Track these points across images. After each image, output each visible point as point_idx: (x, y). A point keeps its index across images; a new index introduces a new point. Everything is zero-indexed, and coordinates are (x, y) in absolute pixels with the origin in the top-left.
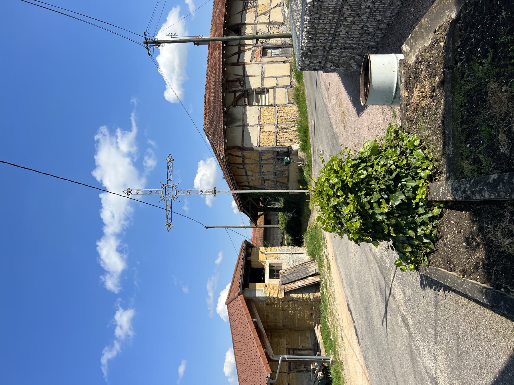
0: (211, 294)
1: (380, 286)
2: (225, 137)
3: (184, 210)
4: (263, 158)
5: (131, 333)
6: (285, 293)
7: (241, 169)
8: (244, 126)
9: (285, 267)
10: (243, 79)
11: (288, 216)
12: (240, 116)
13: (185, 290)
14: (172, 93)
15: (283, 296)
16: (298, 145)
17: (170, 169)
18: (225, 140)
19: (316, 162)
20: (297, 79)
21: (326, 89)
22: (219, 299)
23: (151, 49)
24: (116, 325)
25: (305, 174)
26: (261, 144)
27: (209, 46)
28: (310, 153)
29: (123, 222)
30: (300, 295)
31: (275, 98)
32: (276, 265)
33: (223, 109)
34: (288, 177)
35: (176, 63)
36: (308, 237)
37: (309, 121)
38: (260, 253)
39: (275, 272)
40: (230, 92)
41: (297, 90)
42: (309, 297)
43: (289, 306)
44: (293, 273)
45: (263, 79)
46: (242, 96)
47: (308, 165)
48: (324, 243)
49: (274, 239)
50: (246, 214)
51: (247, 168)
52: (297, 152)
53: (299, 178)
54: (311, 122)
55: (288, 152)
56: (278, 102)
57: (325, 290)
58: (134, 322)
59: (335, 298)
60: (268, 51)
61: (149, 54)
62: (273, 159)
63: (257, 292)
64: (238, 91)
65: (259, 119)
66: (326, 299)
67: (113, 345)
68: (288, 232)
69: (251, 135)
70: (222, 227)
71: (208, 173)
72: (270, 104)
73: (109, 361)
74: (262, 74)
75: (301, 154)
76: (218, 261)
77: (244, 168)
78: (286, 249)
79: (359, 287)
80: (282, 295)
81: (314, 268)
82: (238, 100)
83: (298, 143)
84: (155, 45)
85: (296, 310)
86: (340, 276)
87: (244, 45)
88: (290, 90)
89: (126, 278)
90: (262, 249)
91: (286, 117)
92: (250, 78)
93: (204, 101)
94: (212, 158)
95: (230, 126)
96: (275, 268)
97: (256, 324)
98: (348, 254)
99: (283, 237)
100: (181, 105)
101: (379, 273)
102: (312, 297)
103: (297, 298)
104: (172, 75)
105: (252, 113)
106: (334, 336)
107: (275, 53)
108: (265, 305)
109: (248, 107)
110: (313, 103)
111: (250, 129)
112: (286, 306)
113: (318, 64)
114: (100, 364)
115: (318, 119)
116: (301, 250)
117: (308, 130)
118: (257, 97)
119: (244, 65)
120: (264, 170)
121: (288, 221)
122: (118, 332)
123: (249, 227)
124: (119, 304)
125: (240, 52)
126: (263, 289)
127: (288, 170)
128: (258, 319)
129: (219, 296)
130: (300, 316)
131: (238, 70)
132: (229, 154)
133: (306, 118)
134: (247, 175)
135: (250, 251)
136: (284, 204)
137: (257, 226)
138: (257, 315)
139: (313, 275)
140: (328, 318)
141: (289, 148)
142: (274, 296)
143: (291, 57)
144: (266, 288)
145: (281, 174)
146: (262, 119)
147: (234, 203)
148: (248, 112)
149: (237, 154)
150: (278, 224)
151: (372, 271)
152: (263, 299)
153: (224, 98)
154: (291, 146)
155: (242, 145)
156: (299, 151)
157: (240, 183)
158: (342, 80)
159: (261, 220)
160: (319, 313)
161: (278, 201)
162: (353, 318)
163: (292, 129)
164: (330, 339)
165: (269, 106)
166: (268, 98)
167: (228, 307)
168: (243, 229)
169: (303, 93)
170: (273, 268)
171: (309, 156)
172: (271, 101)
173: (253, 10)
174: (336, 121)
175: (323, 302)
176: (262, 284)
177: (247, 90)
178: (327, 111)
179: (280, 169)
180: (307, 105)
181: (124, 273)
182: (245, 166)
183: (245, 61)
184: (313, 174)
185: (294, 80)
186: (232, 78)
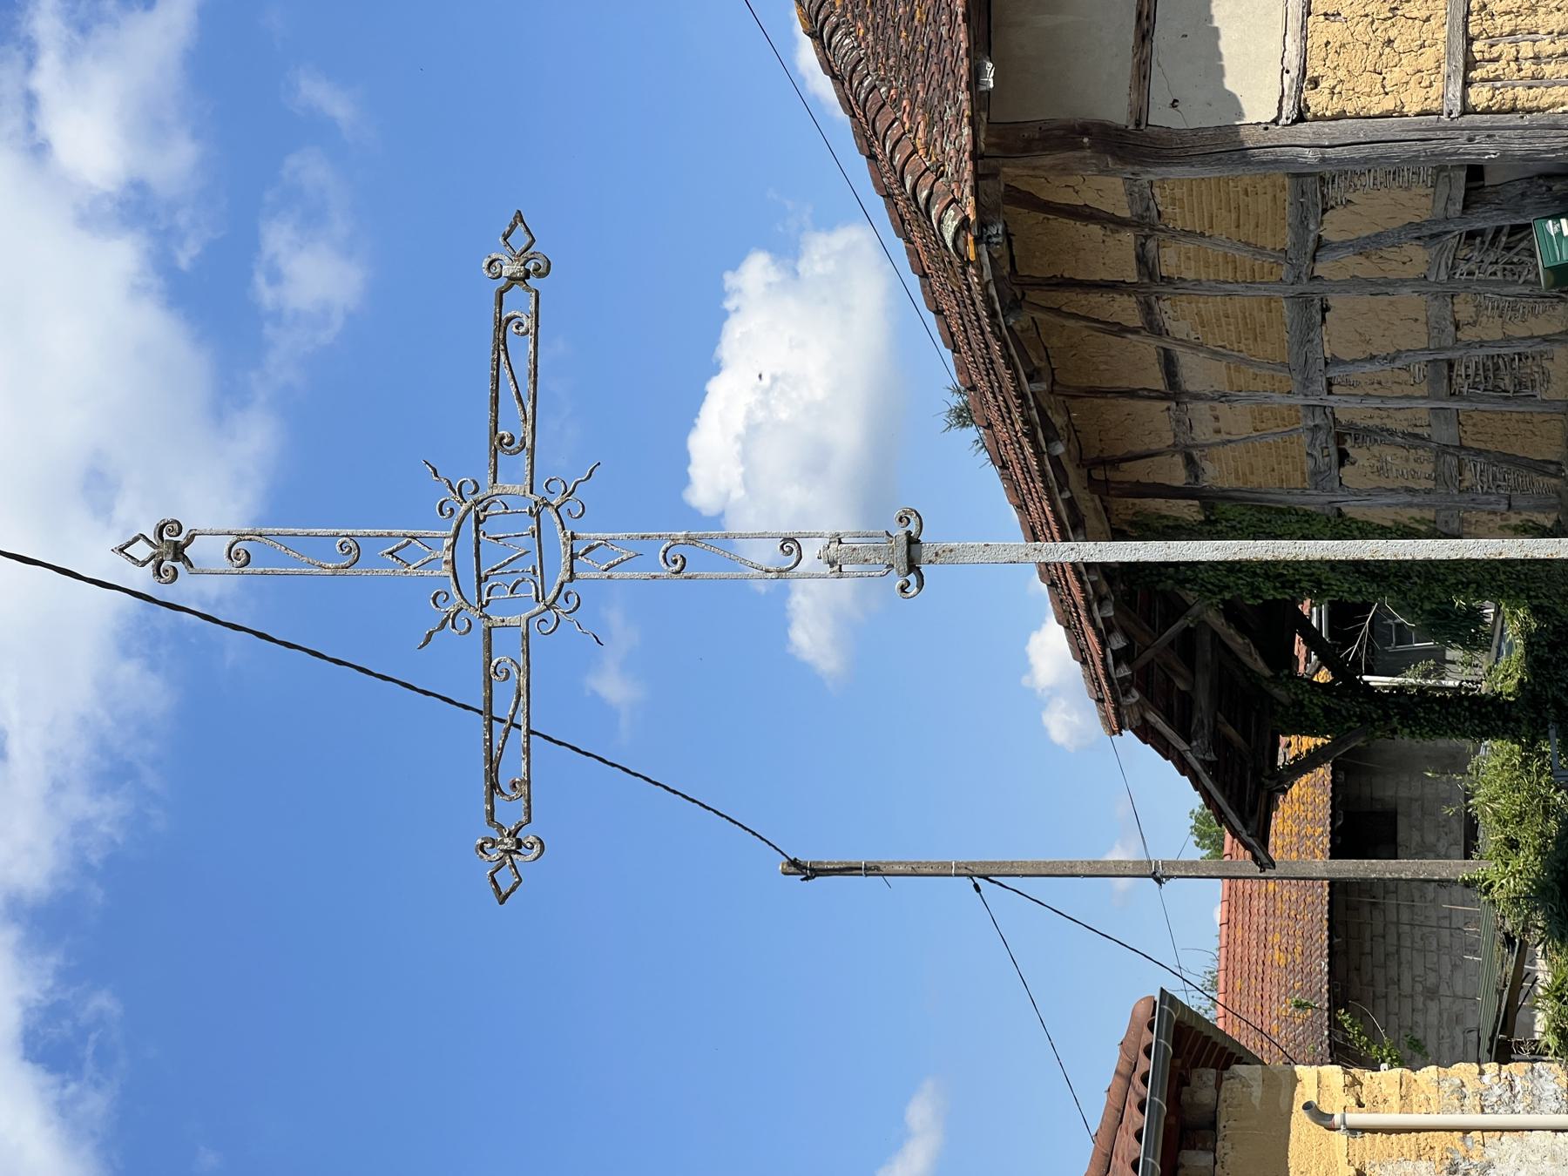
2: (983, 43)
4: (1334, 227)
7: (1121, 330)
17: (521, 350)
18: (976, 74)
26: (1318, 101)
50: (1166, 750)
62: (1426, 234)
70: (941, 871)
71: (811, 370)
77: (1153, 327)
90: (1321, 1082)
99: (1520, 979)
120: (1336, 338)
123: (1191, 871)
132: (1017, 197)
134: (1174, 392)
135: (1206, 1096)
137: (1264, 862)
157: (1115, 462)
159: (1303, 811)
161: (1468, 631)
179: (1491, 329)
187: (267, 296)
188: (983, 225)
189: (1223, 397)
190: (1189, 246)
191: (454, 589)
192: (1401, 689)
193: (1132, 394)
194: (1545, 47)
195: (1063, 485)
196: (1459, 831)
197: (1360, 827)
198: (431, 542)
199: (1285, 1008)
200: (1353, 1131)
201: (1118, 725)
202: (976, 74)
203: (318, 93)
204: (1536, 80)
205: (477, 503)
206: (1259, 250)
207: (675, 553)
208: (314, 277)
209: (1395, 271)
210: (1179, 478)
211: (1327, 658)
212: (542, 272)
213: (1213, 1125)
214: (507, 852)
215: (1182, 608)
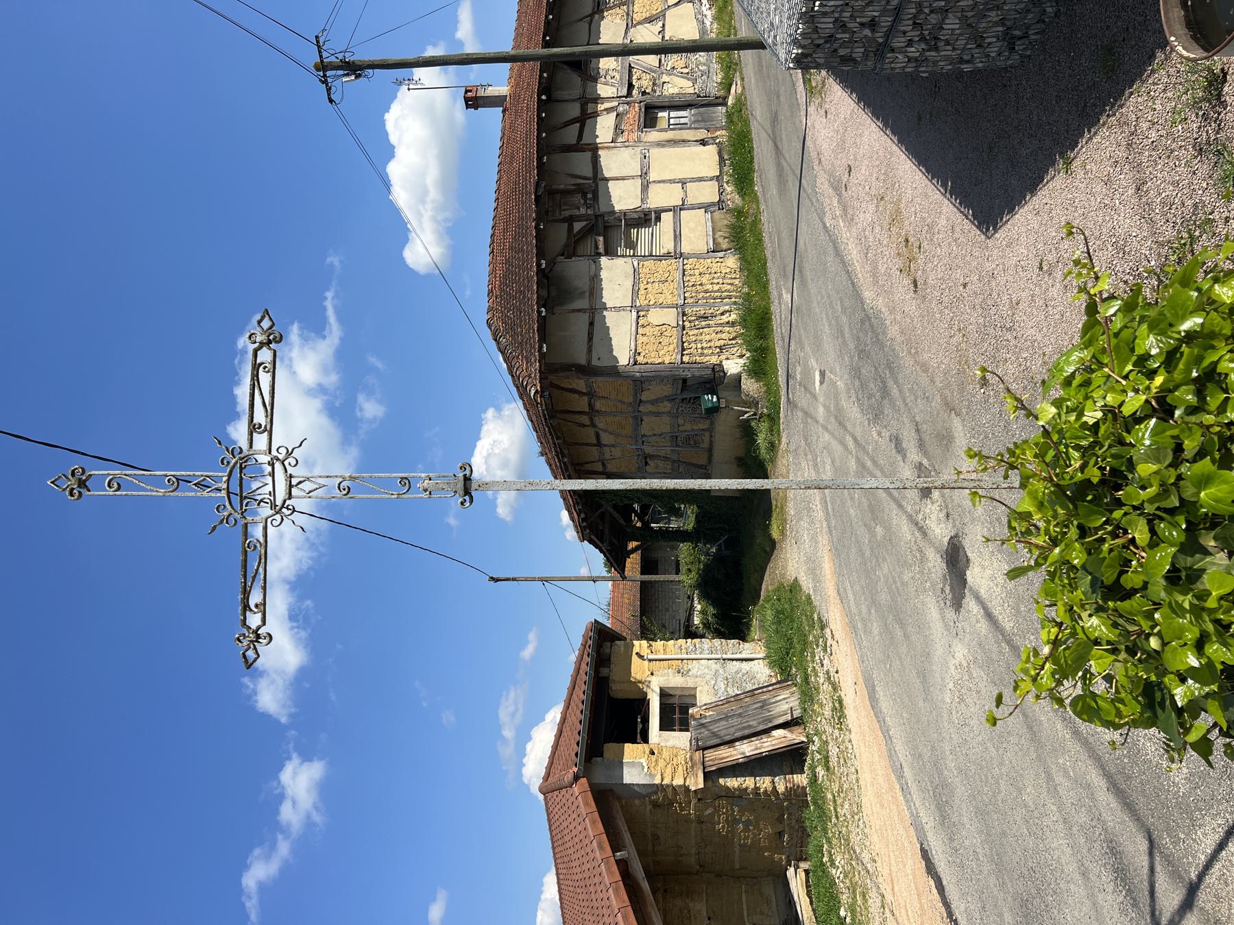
0: (508, 733)
1: (1114, 850)
2: (543, 339)
3: (448, 524)
4: (645, 396)
5: (317, 818)
6: (707, 775)
7: (585, 426)
8: (595, 310)
9: (703, 698)
10: (595, 184)
11: (707, 554)
12: (583, 284)
13: (448, 717)
14: (423, 250)
15: (701, 786)
16: (742, 361)
17: (265, 378)
18: (541, 347)
19: (796, 406)
20: (736, 185)
21: (836, 189)
22: (529, 746)
23: (336, 85)
24: (281, 797)
25: (761, 440)
26: (640, 359)
27: (504, 111)
28: (778, 386)
29: (302, 554)
30: (749, 782)
31: (677, 237)
32: (679, 693)
33: (539, 265)
34: (710, 450)
35: (433, 174)
36: (769, 615)
37: (774, 293)
38: (634, 657)
39: (676, 712)
40: (556, 220)
41: (739, 213)
42: (774, 788)
43: (717, 810)
44: (727, 718)
45: (645, 188)
46: (590, 231)
47: (769, 415)
48: (823, 636)
49: (667, 610)
50: (596, 546)
51: (601, 425)
52: (738, 378)
53: (741, 452)
54: (780, 296)
55: (714, 380)
56: (686, 248)
57: (821, 771)
58: (326, 790)
59: (859, 806)
60: (660, 114)
61: (331, 101)
62: (670, 399)
63: (626, 770)
64: (579, 218)
65: (635, 293)
66: (824, 798)
67: (273, 847)
68: (705, 596)
69: (612, 334)
70: (533, 579)
71: (503, 440)
72: (663, 251)
73: (262, 886)
74: (644, 174)
75: (750, 386)
76: (527, 653)
77: (593, 425)
78: (708, 645)
79: (981, 813)
80: (697, 782)
81: (786, 703)
82: (577, 242)
83: (741, 356)
84: (347, 75)
85: (736, 821)
86: (891, 754)
87: (597, 99)
88: (717, 214)
89: (307, 685)
90: (640, 646)
91: (709, 287)
92: (611, 184)
93: (489, 250)
94: (513, 405)
95: (557, 310)
96: (675, 701)
97: (623, 866)
98: (926, 691)
99: (692, 608)
100: (441, 277)
101: (1106, 798)
102: (781, 788)
103: (739, 789)
104: (421, 207)
105: (615, 277)
106: (852, 909)
107: (677, 121)
108: (649, 807)
109: (604, 261)
110: (788, 244)
111: (610, 318)
112: (709, 811)
113: (867, 32)
114: (239, 890)
115: (804, 283)
116: (747, 649)
117: (770, 320)
118: (628, 235)
119: (594, 149)
120: (645, 429)
121: (706, 566)
122: (288, 814)
123: (604, 579)
124: (291, 746)
125: (586, 117)
126: (644, 761)
127: (711, 430)
128: (629, 852)
129: (530, 738)
130: (746, 838)
131: (580, 165)
132: (552, 385)
133: (765, 286)
134: (599, 444)
135: (607, 651)
136: (698, 520)
137: (624, 578)
138: (627, 838)
139: (784, 726)
140: (830, 855)
141: (717, 369)
142: (675, 783)
143: (722, 128)
144: (653, 758)
145: (691, 441)
146: (642, 292)
147: (565, 515)
148: (603, 274)
149: (574, 386)
150: (678, 572)
151: (1059, 779)
152: (643, 792)
153: (540, 236)
154: (720, 365)
155: (589, 362)
156: (744, 376)
157: (582, 464)
158: (901, 141)
159: (633, 563)
160: (803, 835)
161: (678, 513)
162: (947, 905)
163: (725, 318)
164: (839, 917)
165: (660, 258)
166: (662, 236)
167: (545, 799)
168: (590, 589)
169: (756, 222)
170: (671, 701)
171: (772, 392)
172: (668, 245)
173: (621, 11)
174: (875, 275)
175: (815, 803)
176: (640, 747)
177: (602, 216)
178: (838, 253)
179: (688, 427)
180: (768, 254)
181: (303, 674)
182: (596, 419)
183: (598, 141)
184: (784, 440)
185: (729, 189)
186: (564, 183)
187: (358, 414)
188: (542, 391)
189: (613, 446)
190: (604, 401)
191: (227, 503)
192: (335, 307)
193: (587, 444)
194: (705, 345)
195: (567, 470)
196: (674, 565)
197: (648, 567)
198: (217, 479)
199: (628, 615)
200: (650, 660)
201: (583, 539)
202: (541, 347)
203: (373, 360)
204: (702, 354)
205: (241, 459)
206: (623, 402)
207: (344, 484)
208: (371, 409)
209: (662, 409)
210: (600, 469)
211: (640, 519)
212: (279, 340)
213: (609, 660)
214: (252, 641)
215: (602, 506)
